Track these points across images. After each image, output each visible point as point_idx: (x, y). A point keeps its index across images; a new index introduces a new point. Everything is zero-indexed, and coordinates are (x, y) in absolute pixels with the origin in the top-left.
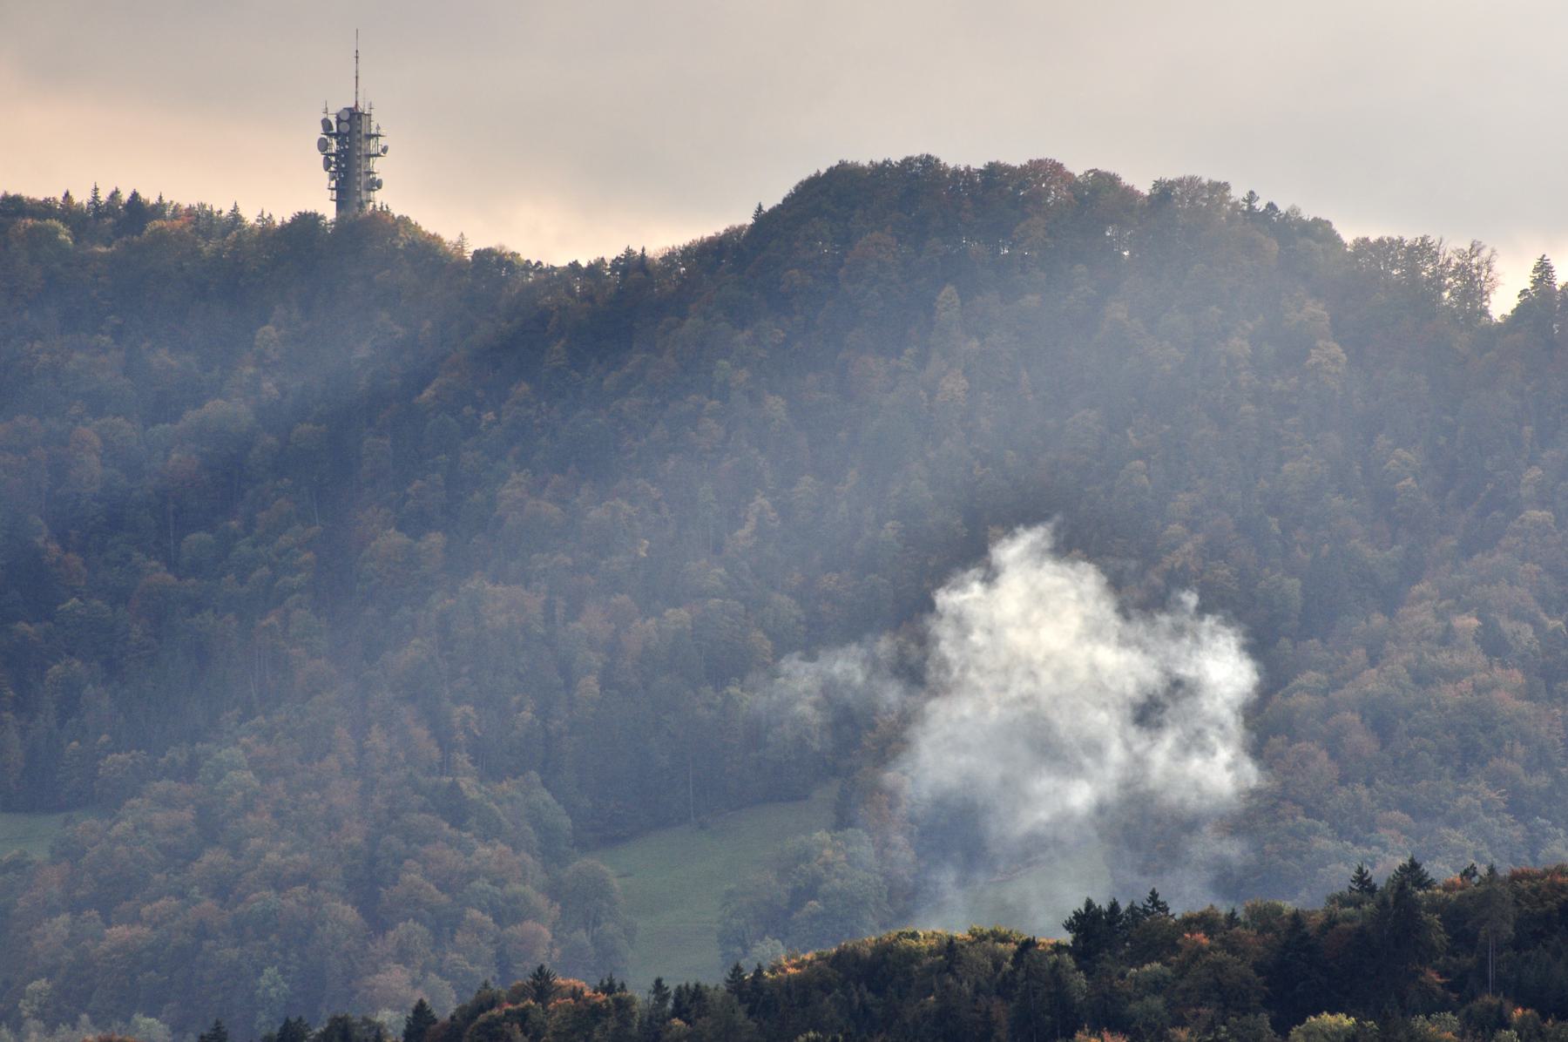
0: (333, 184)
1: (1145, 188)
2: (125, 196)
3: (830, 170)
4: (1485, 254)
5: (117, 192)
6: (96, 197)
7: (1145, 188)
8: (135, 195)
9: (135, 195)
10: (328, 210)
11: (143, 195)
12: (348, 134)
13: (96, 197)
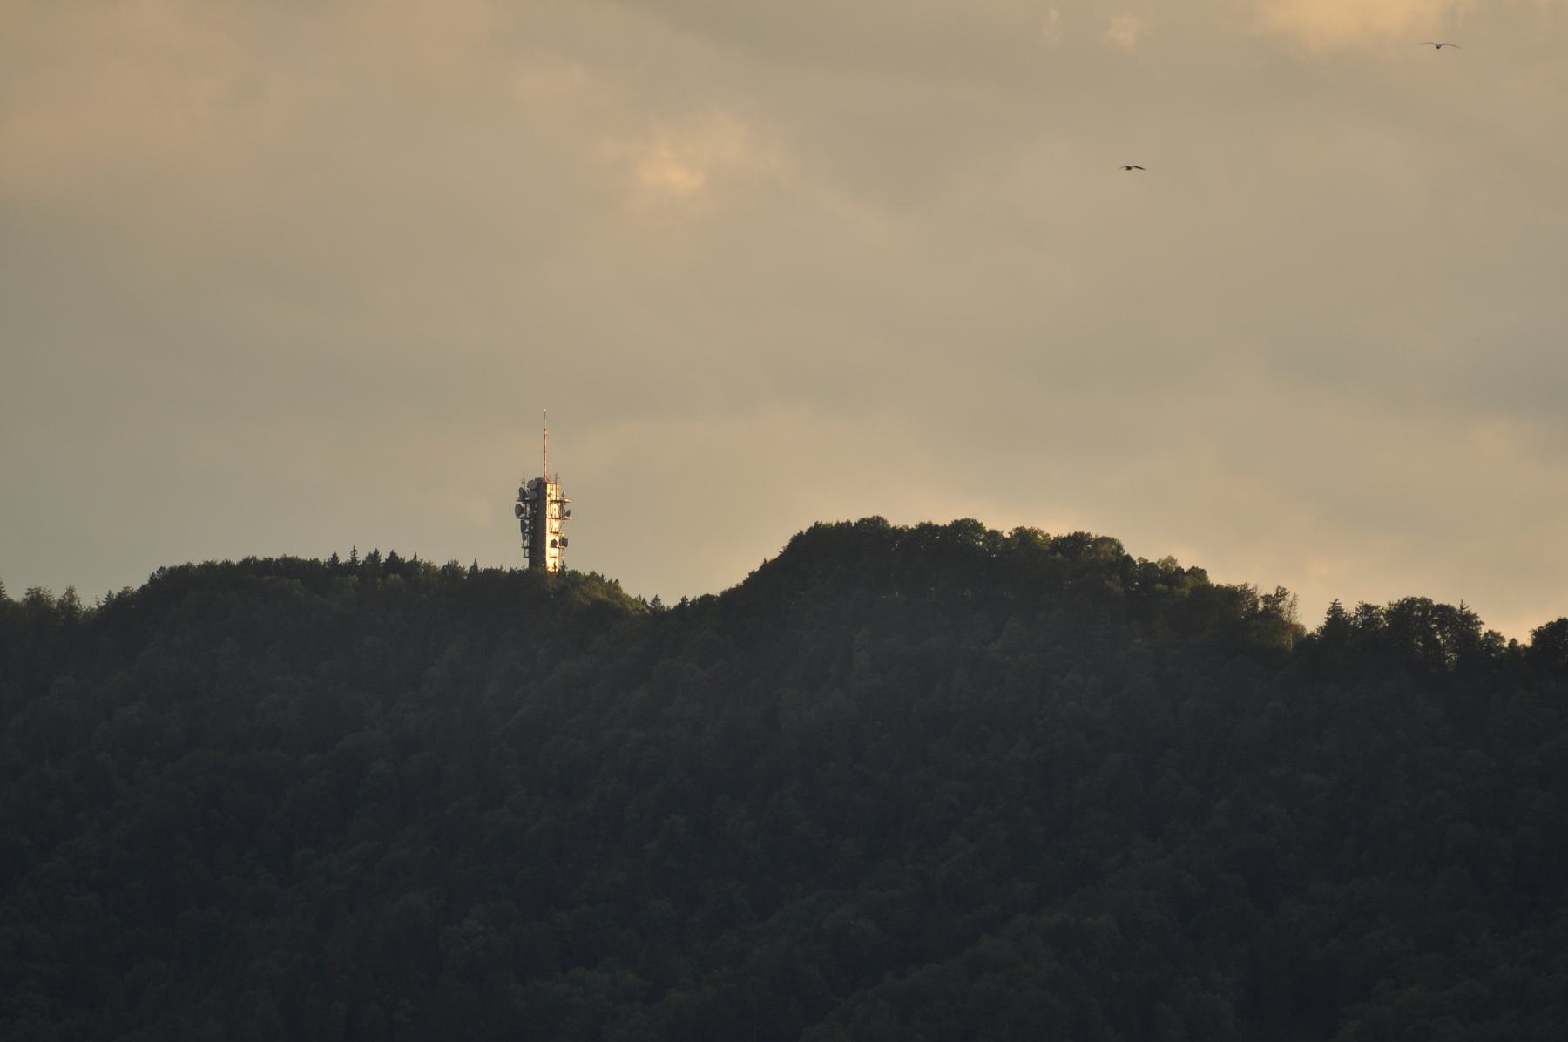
0: (526, 543)
1: (1525, 639)
2: (384, 557)
3: (810, 530)
4: (1289, 598)
5: (376, 553)
6: (354, 559)
7: (1525, 639)
8: (393, 554)
9: (393, 554)
10: (522, 563)
11: (400, 555)
12: (537, 500)
13: (354, 559)
